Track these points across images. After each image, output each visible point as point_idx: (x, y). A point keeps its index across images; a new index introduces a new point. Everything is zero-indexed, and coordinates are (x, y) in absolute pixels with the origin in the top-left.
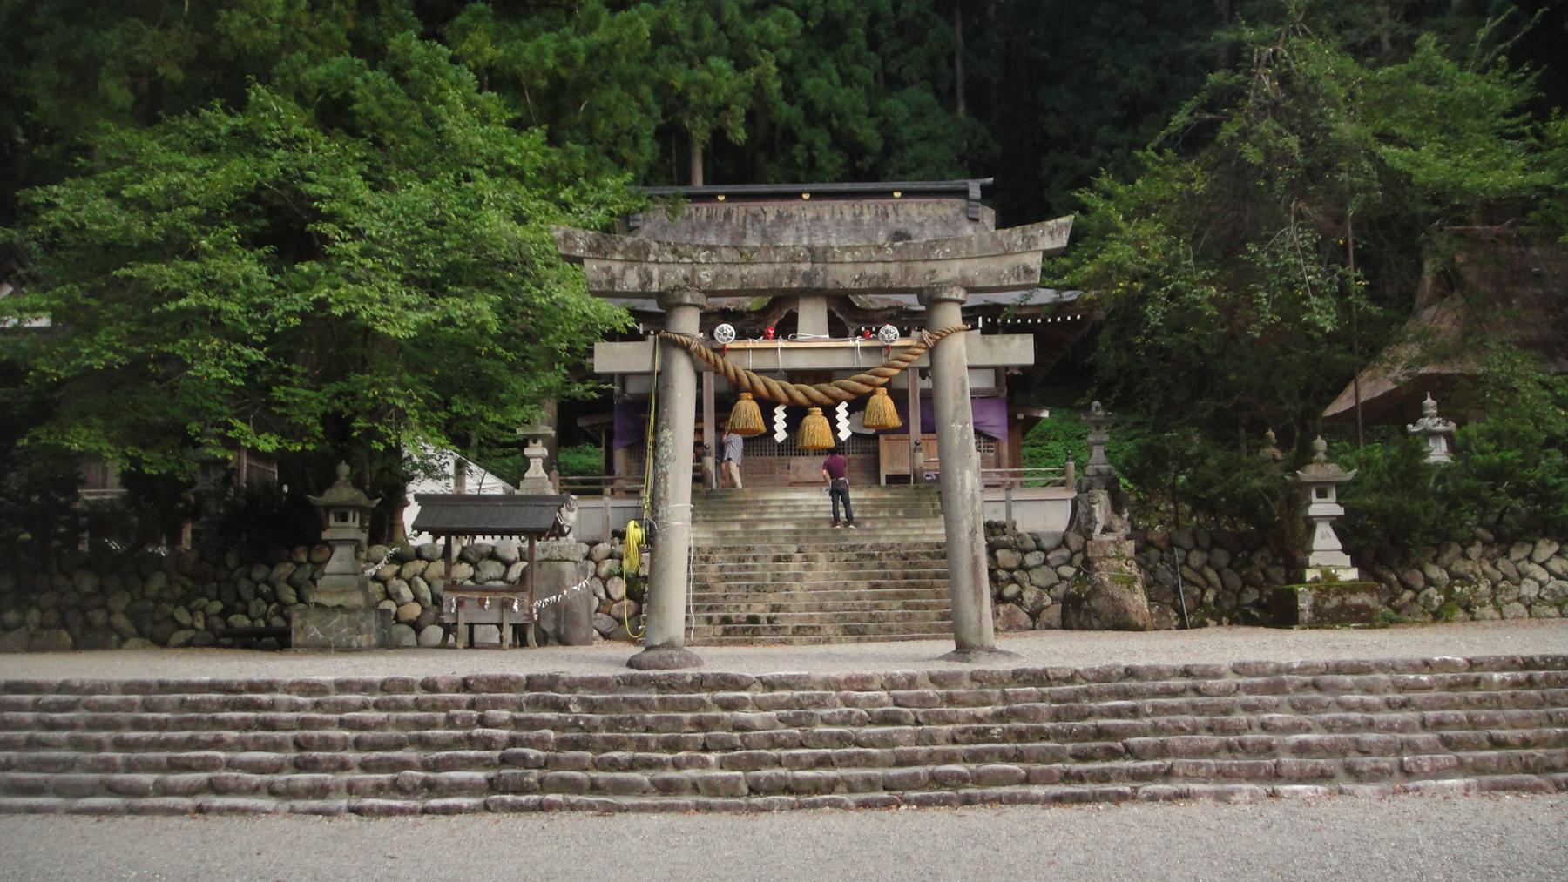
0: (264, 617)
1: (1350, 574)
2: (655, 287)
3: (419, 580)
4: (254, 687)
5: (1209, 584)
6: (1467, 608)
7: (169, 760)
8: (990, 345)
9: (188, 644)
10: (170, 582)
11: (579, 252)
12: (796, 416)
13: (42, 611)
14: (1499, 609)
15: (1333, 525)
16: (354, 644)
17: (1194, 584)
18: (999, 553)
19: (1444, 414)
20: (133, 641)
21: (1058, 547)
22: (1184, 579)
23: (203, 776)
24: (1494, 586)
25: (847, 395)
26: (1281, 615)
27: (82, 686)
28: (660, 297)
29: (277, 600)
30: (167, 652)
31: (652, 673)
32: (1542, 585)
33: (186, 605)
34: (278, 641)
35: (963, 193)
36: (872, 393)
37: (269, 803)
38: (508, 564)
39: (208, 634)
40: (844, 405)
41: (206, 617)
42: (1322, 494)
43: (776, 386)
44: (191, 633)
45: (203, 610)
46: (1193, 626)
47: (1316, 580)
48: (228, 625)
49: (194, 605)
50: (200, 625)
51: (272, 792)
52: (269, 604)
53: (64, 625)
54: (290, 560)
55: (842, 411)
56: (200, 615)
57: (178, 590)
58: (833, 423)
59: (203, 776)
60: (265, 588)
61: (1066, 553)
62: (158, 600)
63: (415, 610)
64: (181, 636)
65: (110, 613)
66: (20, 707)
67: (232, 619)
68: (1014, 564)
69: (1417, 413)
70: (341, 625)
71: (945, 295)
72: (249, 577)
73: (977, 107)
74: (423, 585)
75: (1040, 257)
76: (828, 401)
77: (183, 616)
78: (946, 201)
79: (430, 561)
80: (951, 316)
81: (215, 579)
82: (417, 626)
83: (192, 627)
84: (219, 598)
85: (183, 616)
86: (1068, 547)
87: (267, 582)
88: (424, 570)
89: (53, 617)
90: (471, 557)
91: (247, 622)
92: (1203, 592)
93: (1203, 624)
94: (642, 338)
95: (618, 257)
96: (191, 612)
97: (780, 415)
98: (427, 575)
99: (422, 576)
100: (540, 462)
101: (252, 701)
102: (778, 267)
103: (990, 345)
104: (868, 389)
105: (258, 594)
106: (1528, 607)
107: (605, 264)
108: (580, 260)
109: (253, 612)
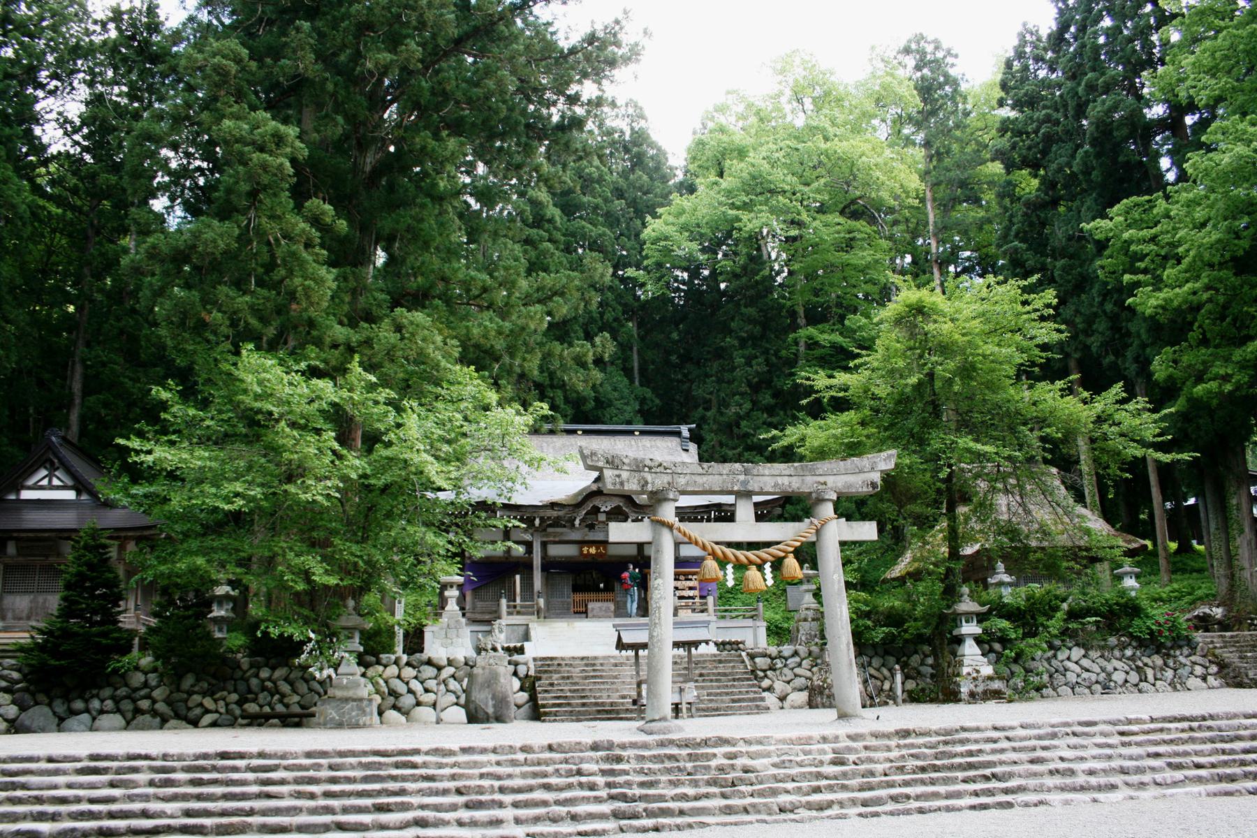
0: (269, 704)
1: (988, 670)
2: (650, 488)
3: (451, 680)
4: (224, 756)
6: (1038, 689)
7: (374, 805)
9: (214, 724)
10: (198, 680)
11: (600, 464)
13: (102, 701)
14: (1054, 689)
16: (361, 723)
19: (1008, 571)
20: (173, 722)
21: (793, 656)
24: (1051, 676)
26: (952, 696)
28: (653, 494)
29: (278, 692)
30: (196, 730)
32: (1078, 676)
34: (296, 720)
35: (678, 434)
39: (229, 717)
40: (769, 564)
41: (227, 705)
42: (220, 604)
43: (729, 551)
44: (216, 716)
45: (224, 699)
46: (880, 705)
48: (243, 711)
49: (217, 696)
50: (223, 710)
52: (272, 696)
53: (118, 710)
54: (287, 665)
55: (767, 566)
56: (222, 703)
57: (205, 685)
58: (763, 575)
60: (269, 684)
61: (797, 659)
64: (208, 718)
65: (154, 702)
67: (246, 706)
69: (992, 570)
70: (352, 710)
72: (257, 676)
73: (646, 380)
74: (381, 682)
76: (758, 561)
78: (667, 438)
79: (385, 666)
80: (828, 510)
81: (232, 678)
83: (217, 711)
84: (235, 691)
85: (208, 703)
89: (109, 704)
91: (257, 708)
93: (886, 703)
94: (641, 520)
96: (216, 701)
100: (454, 600)
104: (782, 554)
105: (264, 689)
106: (1073, 689)
107: (617, 472)
109: (261, 701)
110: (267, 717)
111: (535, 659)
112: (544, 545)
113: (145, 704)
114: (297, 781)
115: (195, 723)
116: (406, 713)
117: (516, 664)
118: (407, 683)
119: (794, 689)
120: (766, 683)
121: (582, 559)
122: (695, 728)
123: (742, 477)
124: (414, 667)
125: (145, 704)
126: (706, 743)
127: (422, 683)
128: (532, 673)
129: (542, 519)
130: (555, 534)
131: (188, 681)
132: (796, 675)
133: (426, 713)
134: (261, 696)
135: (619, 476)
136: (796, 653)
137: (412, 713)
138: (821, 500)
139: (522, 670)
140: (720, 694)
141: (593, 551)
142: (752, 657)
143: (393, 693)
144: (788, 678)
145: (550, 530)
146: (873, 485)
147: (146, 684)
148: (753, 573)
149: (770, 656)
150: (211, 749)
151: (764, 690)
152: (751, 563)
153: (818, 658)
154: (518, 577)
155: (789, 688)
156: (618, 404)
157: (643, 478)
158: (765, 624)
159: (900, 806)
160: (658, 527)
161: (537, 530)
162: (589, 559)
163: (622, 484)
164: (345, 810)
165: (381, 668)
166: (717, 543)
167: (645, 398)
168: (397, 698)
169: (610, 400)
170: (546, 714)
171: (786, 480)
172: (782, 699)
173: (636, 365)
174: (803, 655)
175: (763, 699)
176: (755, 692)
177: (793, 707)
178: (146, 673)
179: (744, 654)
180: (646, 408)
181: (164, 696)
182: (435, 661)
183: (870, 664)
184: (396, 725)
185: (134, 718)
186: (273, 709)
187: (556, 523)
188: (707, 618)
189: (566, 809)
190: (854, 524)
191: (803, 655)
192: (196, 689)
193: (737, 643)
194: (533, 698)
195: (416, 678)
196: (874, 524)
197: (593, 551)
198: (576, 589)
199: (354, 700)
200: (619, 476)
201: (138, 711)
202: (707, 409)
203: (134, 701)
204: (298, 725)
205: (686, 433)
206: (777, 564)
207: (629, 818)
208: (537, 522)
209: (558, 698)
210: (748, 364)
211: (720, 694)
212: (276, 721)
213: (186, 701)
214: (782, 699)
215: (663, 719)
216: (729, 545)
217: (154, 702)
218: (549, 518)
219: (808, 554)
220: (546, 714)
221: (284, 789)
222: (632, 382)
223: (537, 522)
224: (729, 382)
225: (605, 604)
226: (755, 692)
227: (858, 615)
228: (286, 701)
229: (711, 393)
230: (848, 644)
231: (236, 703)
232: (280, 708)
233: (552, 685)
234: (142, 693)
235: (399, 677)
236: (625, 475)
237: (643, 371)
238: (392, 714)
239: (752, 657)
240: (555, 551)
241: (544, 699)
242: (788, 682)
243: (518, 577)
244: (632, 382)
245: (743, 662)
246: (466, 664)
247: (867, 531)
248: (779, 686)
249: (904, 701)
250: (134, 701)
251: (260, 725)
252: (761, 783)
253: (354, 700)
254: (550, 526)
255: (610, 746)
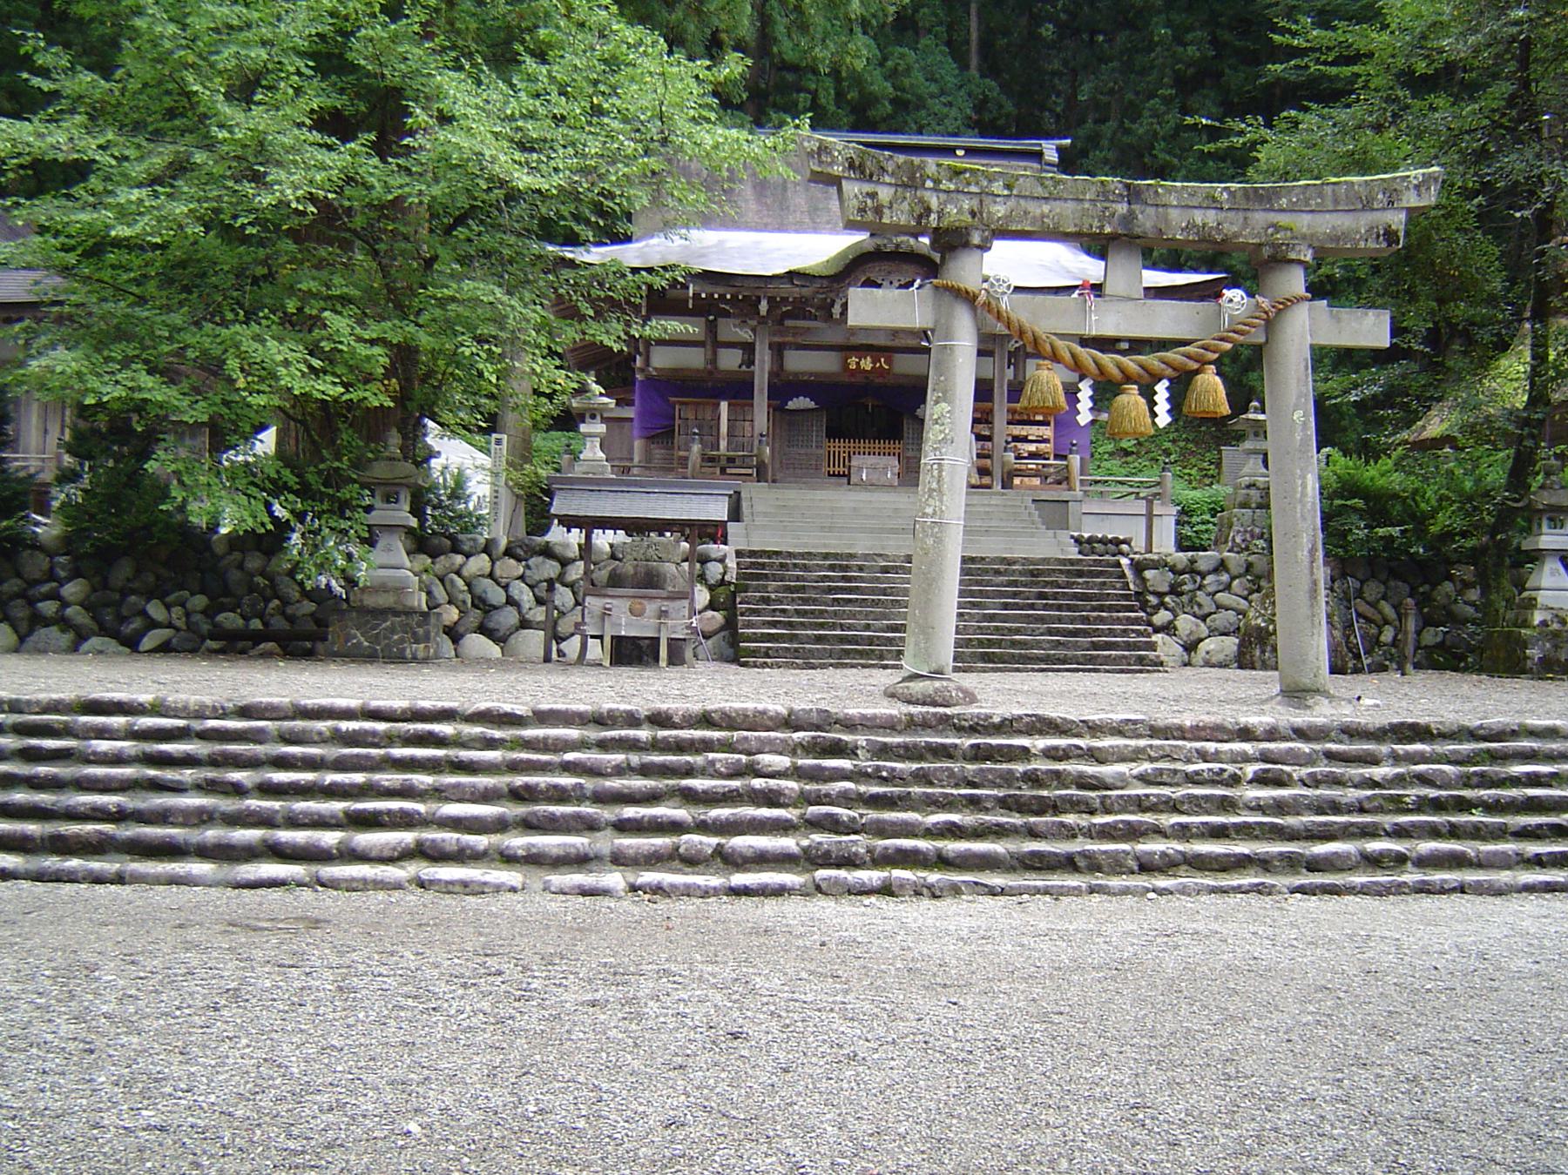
0: (261, 616)
3: (455, 577)
5: (1387, 622)
7: (347, 813)
8: (1339, 320)
9: (165, 649)
10: (138, 571)
11: (837, 170)
12: (1106, 391)
15: (1562, 560)
17: (1369, 620)
18: (1148, 574)
20: (95, 642)
21: (1216, 571)
22: (1359, 615)
23: (408, 837)
25: (1169, 372)
27: (185, 708)
28: (937, 234)
31: (948, 711)
33: (161, 598)
36: (1197, 372)
37: (511, 877)
38: (565, 563)
40: (1165, 383)
41: (188, 615)
43: (1085, 354)
44: (167, 633)
45: (183, 605)
47: (1544, 623)
48: (215, 625)
50: (181, 624)
51: (508, 859)
52: (267, 601)
56: (177, 611)
57: (151, 579)
58: (1152, 404)
59: (408, 837)
61: (1225, 577)
62: (125, 592)
63: (452, 614)
65: (65, 604)
66: (103, 733)
67: (220, 618)
68: (1166, 588)
70: (393, 630)
71: (1293, 256)
73: (991, 68)
74: (460, 583)
75: (1403, 216)
77: (156, 610)
79: (468, 556)
80: (1294, 282)
82: (454, 634)
83: (170, 625)
85: (156, 610)
86: (1227, 571)
87: (263, 574)
88: (461, 566)
90: (520, 552)
91: (241, 622)
92: (1380, 628)
95: (887, 179)
96: (168, 607)
97: (1085, 392)
98: (465, 572)
99: (458, 573)
101: (431, 733)
102: (1087, 205)
103: (1339, 320)
104: (1195, 366)
105: (252, 588)
107: (868, 188)
108: (836, 181)
110: (257, 638)
111: (739, 554)
112: (778, 350)
113: (48, 608)
114: (215, 762)
115: (132, 644)
116: (500, 639)
117: (704, 560)
118: (506, 587)
119: (1214, 632)
120: (1162, 617)
121: (846, 379)
122: (1001, 694)
123: (1122, 208)
124: (519, 560)
125: (48, 608)
126: (1007, 726)
127: (531, 587)
128: (731, 576)
129: (771, 300)
130: (796, 331)
131: (123, 571)
132: (1218, 607)
133: (533, 641)
134: (246, 600)
135: (873, 195)
136: (1221, 566)
137: (512, 640)
138: (1279, 260)
139: (714, 570)
140: (1075, 633)
141: (867, 364)
142: (1138, 568)
143: (480, 603)
144: (1206, 610)
145: (789, 323)
146: (1390, 235)
147: (51, 576)
148: (1132, 398)
149: (1173, 569)
150: (67, 694)
151: (1157, 630)
152: (1128, 378)
153: (1259, 580)
154: (724, 405)
155: (1203, 629)
156: (936, 105)
157: (921, 201)
158: (1174, 510)
159: (1382, 878)
160: (947, 298)
161: (763, 321)
162: (859, 379)
163: (878, 210)
164: (293, 822)
165: (459, 559)
166: (1062, 336)
167: (986, 100)
168: (486, 612)
169: (920, 98)
170: (754, 653)
171: (1210, 218)
172: (1190, 647)
173: (974, 36)
174: (1235, 570)
175: (1152, 646)
176: (1139, 633)
177: (1208, 664)
178: (51, 556)
179: (1124, 561)
180: (987, 117)
181: (81, 596)
182: (558, 550)
183: (1359, 594)
184: (485, 663)
185: (31, 632)
186: (265, 624)
187: (800, 309)
188: (1065, 496)
189: (714, 841)
190: (1344, 313)
191: (1235, 570)
192: (136, 585)
193: (1117, 542)
194: (730, 624)
195: (522, 578)
196: (1385, 317)
197: (867, 364)
198: (832, 434)
199: (396, 613)
200: (873, 195)
201: (38, 620)
202: (1103, 121)
203: (31, 603)
204: (308, 655)
205: (1051, 155)
206: (1182, 383)
207: (838, 866)
208: (764, 307)
209: (774, 624)
210: (1179, 40)
211: (1075, 633)
212: (270, 645)
213: (119, 604)
214: (1190, 647)
215: (938, 673)
216: (1085, 342)
217: (65, 604)
218: (784, 300)
219: (1245, 368)
220: (754, 653)
221: (188, 775)
222: (964, 66)
223: (764, 307)
224: (1143, 72)
225: (884, 460)
226: (1139, 633)
227: (1340, 504)
228: (289, 611)
229: (1111, 92)
230: (1312, 551)
231: (204, 612)
232: (279, 623)
233: (767, 601)
234: (45, 588)
235: (491, 576)
236: (885, 194)
237: (986, 46)
238: (477, 643)
239: (1138, 568)
240: (799, 362)
241: (749, 625)
242: (1204, 618)
243: (724, 405)
244: (964, 66)
245: (1123, 575)
246: (613, 557)
247: (1370, 328)
248: (1185, 623)
249: (1417, 666)
250: (31, 603)
251: (243, 652)
252: (1108, 812)
253: (396, 613)
254: (788, 315)
255: (826, 721)
